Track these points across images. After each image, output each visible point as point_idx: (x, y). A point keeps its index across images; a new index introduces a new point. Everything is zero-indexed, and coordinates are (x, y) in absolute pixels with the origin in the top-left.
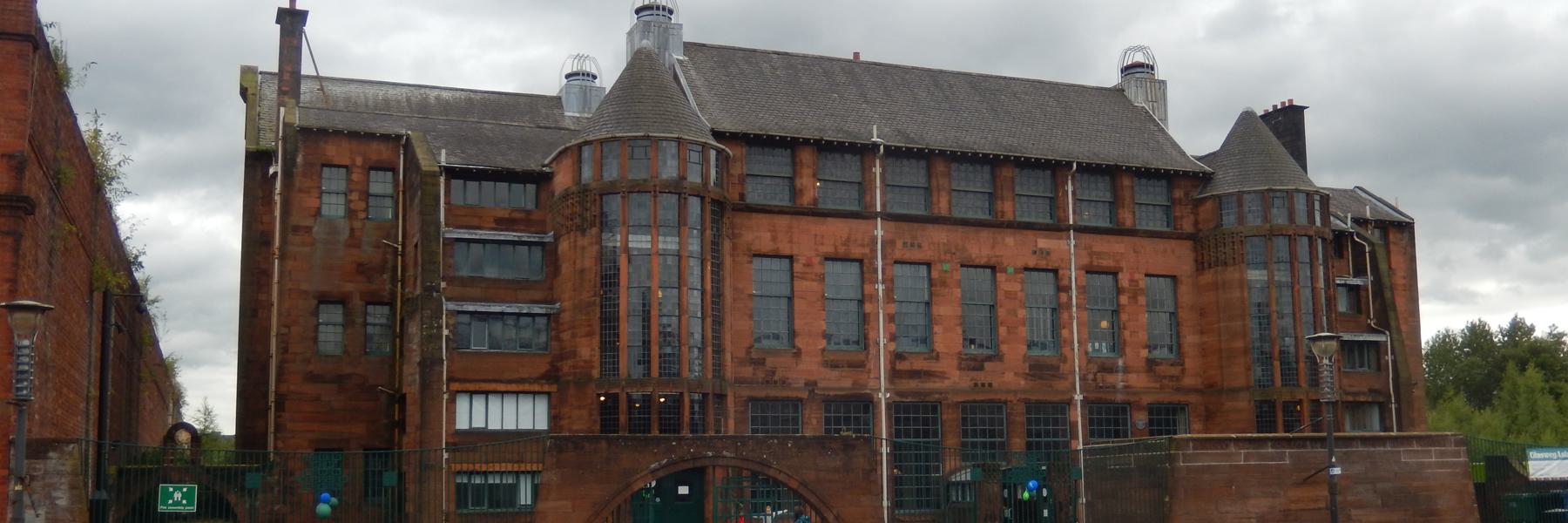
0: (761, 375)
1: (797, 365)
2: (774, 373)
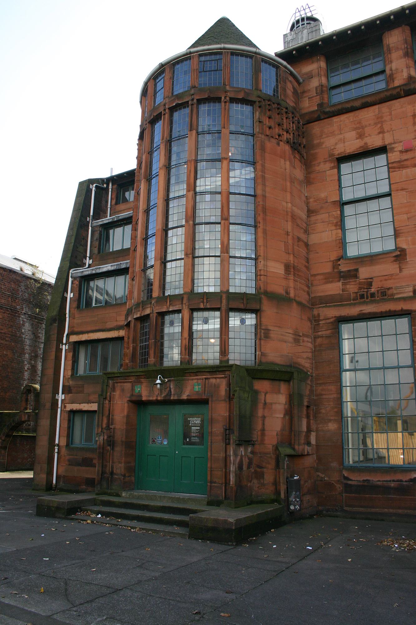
0: (352, 288)
1: (401, 270)
2: (370, 284)
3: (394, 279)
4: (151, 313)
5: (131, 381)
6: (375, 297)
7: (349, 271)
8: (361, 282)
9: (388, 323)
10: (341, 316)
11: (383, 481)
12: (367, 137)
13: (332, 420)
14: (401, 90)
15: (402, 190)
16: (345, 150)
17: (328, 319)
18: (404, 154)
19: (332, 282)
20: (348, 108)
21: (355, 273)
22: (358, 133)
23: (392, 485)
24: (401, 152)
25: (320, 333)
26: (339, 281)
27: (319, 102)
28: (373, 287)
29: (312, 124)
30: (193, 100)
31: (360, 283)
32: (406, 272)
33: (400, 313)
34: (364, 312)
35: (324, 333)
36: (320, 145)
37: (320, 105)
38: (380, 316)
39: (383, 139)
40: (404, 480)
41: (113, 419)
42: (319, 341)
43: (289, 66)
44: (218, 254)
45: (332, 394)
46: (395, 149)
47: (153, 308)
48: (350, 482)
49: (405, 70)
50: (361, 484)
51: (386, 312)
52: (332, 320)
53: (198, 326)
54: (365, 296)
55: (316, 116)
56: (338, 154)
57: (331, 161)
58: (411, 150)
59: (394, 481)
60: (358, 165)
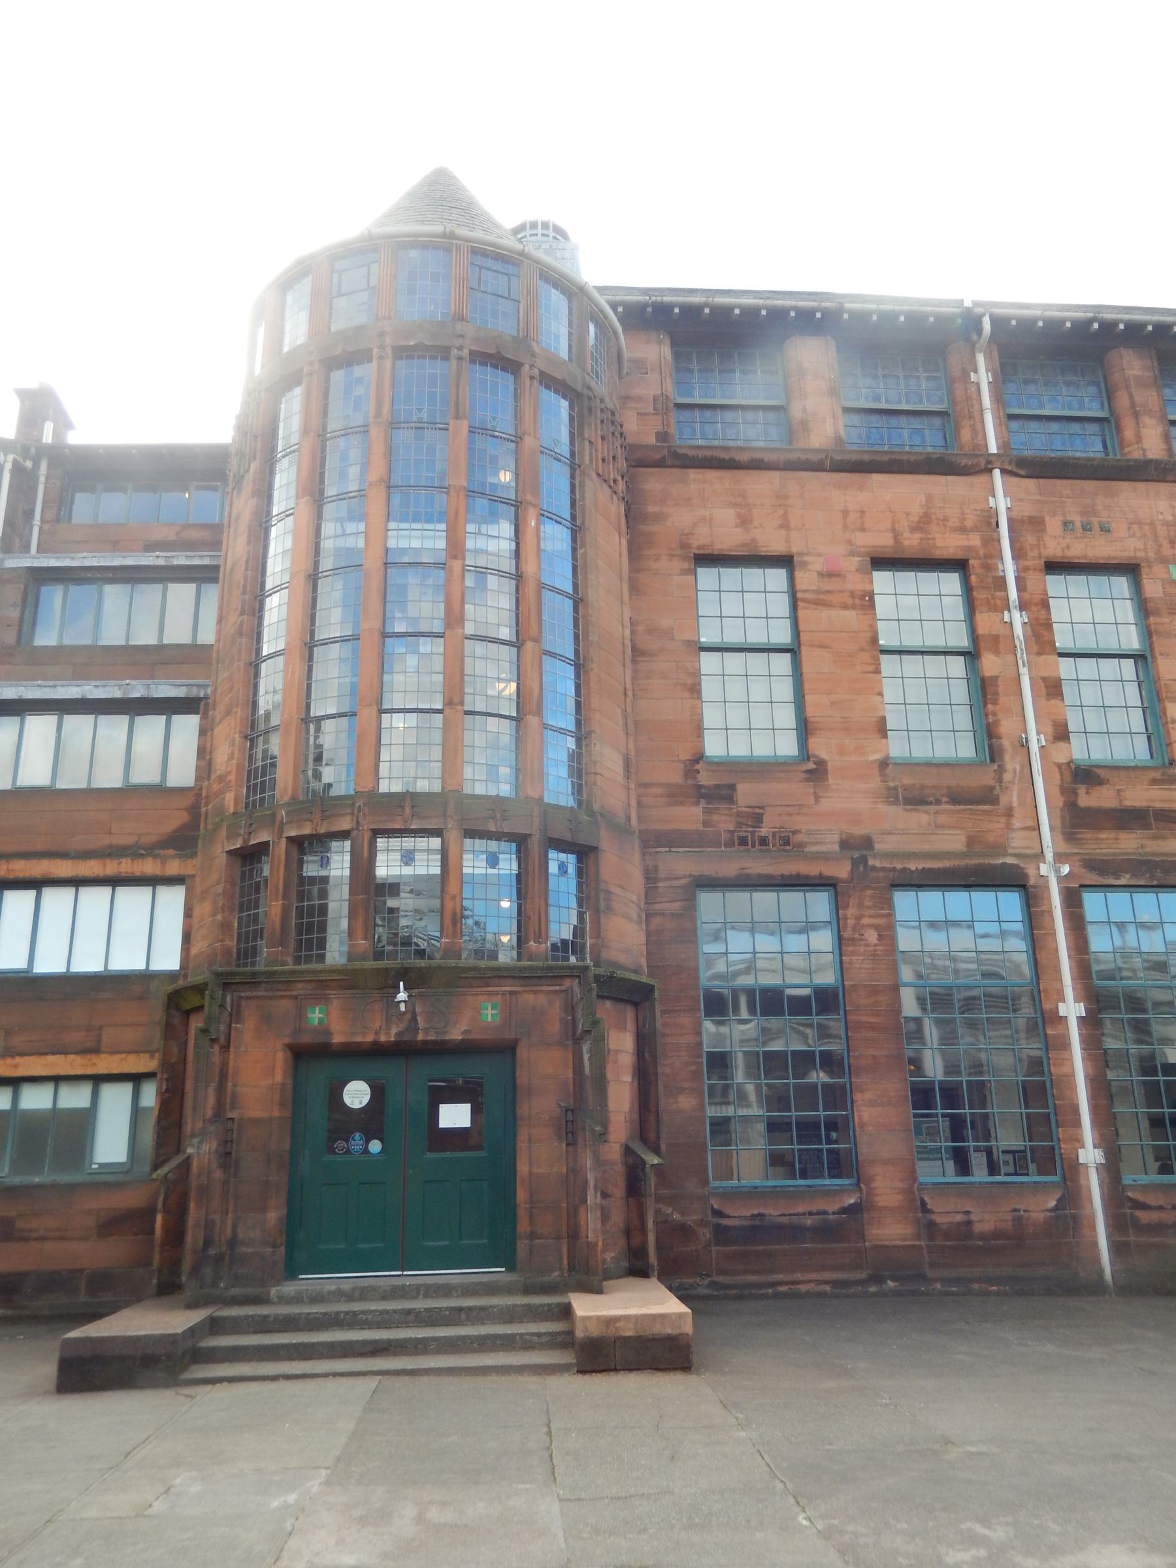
0: (724, 823)
1: (817, 798)
2: (758, 819)
3: (805, 814)
4: (353, 829)
5: (294, 993)
6: (768, 845)
7: (717, 787)
8: (741, 812)
9: (792, 900)
10: (702, 876)
11: (790, 1215)
12: (756, 528)
13: (686, 1089)
14: (827, 457)
15: (821, 646)
16: (712, 542)
17: (677, 878)
18: (826, 580)
19: (682, 804)
20: (724, 459)
21: (729, 792)
22: (739, 516)
23: (809, 1221)
24: (820, 574)
25: (658, 906)
26: (698, 803)
27: (660, 428)
28: (764, 825)
29: (644, 469)
30: (461, 348)
31: (739, 814)
32: (827, 804)
33: (818, 882)
34: (748, 871)
35: (666, 906)
36: (659, 517)
37: (663, 436)
38: (779, 882)
39: (788, 540)
40: (830, 1211)
41: (234, 1096)
42: (656, 921)
43: (622, 337)
44: (439, 706)
45: (685, 1034)
46: (810, 567)
47: (357, 817)
48: (725, 1222)
49: (829, 421)
50: (748, 1223)
51: (791, 877)
52: (684, 881)
53: (387, 867)
54: (750, 842)
55: (658, 456)
56: (699, 548)
57: (684, 558)
58: (838, 575)
59: (811, 1213)
60: (731, 576)
